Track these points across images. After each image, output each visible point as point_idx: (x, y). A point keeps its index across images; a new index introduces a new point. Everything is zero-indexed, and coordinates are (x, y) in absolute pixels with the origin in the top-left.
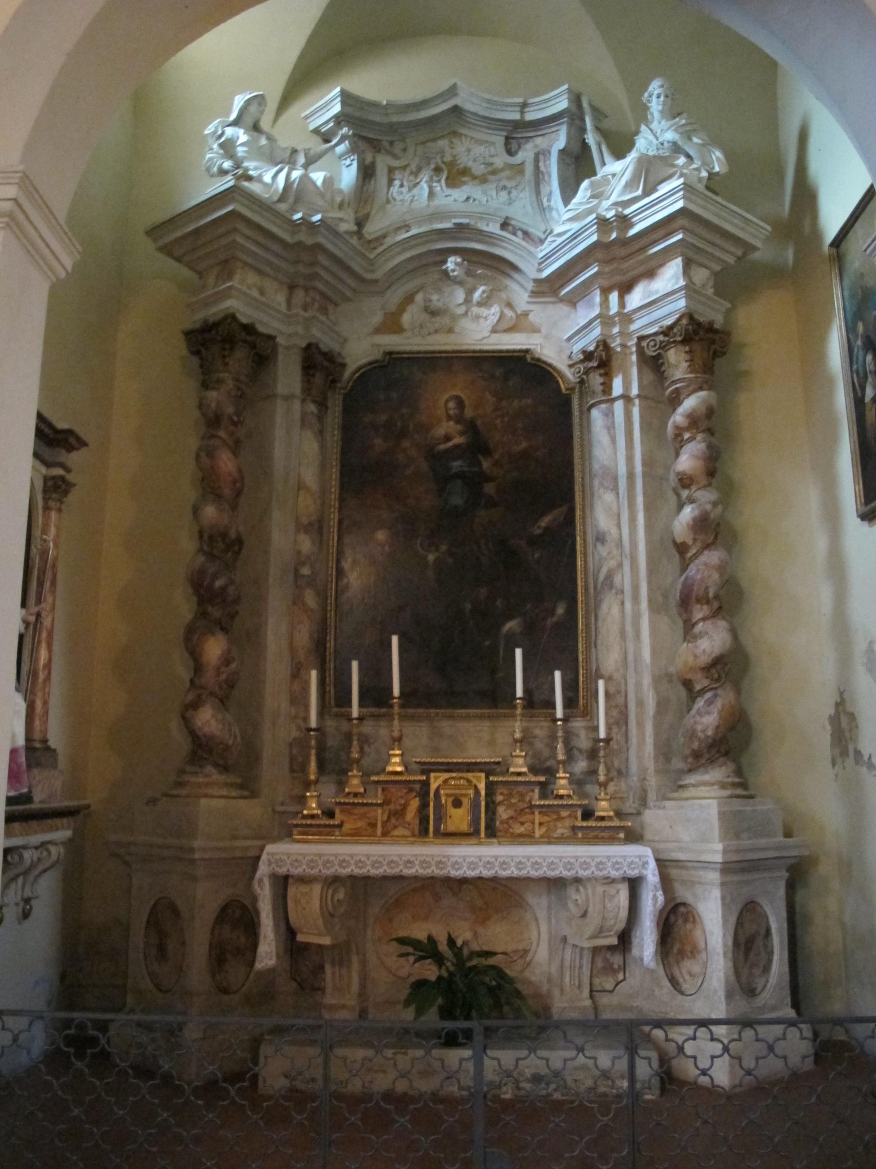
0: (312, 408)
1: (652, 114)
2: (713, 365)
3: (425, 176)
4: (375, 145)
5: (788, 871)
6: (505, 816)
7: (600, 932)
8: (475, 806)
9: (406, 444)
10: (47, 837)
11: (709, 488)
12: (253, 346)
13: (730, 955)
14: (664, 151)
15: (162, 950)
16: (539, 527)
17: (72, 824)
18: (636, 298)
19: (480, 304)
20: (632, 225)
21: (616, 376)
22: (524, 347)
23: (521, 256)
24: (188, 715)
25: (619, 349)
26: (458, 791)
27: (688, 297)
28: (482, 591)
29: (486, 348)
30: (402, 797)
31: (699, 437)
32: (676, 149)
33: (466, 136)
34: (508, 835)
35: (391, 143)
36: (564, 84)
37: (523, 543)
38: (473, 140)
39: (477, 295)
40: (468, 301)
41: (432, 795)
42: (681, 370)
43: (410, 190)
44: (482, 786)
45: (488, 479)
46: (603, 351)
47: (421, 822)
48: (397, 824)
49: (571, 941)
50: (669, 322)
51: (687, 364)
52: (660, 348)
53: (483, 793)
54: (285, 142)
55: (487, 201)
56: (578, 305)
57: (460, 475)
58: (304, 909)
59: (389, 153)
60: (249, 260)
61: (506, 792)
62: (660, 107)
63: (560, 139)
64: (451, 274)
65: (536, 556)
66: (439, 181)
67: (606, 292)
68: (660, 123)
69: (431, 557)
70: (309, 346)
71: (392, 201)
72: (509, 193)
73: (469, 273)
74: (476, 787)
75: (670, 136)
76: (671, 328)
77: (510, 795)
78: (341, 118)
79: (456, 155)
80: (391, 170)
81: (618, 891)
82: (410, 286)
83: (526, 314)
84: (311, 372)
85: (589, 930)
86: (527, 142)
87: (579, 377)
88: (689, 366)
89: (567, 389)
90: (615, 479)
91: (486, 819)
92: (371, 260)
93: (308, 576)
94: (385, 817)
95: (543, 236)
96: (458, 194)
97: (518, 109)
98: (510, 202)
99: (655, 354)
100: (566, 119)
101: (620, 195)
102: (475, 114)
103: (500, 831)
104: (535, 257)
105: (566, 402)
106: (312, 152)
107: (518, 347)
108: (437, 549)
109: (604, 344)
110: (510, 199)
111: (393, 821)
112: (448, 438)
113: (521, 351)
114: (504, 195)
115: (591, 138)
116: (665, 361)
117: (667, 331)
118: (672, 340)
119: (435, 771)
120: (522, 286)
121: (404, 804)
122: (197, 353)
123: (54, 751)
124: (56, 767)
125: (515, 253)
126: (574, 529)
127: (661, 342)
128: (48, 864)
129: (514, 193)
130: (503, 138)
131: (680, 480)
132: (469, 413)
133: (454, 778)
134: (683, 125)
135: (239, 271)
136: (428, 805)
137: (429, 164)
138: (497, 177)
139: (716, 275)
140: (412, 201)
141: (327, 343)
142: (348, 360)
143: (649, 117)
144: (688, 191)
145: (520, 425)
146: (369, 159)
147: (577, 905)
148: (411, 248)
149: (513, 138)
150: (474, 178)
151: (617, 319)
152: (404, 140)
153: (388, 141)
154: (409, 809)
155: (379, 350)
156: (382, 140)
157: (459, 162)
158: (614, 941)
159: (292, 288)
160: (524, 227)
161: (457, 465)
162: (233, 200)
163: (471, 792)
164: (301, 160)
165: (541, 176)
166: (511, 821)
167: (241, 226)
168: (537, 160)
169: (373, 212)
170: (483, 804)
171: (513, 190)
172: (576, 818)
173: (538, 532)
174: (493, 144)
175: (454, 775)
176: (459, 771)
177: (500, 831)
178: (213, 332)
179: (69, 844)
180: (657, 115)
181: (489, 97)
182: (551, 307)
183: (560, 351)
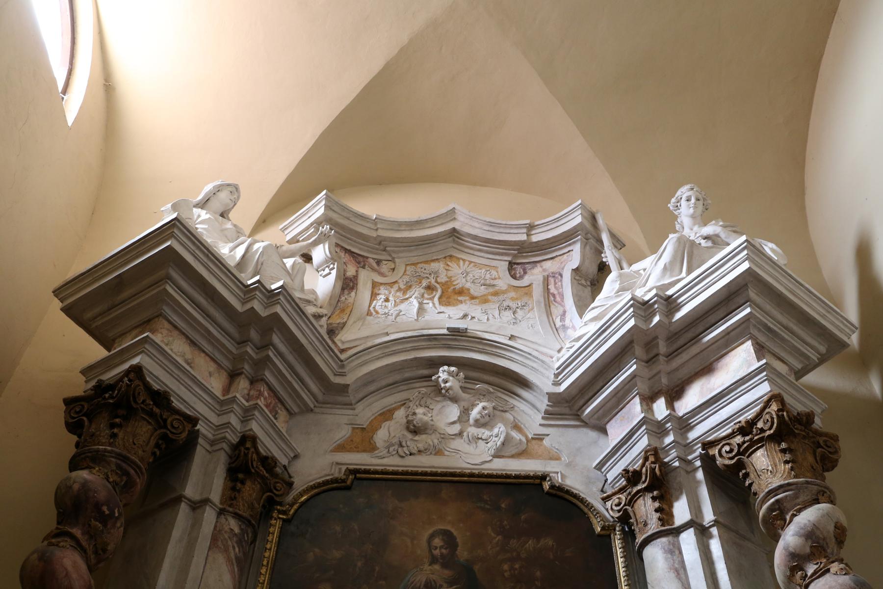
0: (233, 524)
3: (417, 291)
4: (360, 260)
19: (478, 424)
20: (678, 308)
21: (677, 499)
33: (464, 260)
35: (379, 262)
39: (475, 413)
50: (750, 415)
51: (788, 466)
55: (488, 319)
56: (608, 427)
59: (373, 269)
62: (691, 211)
66: (432, 299)
67: (648, 400)
71: (374, 313)
72: (514, 313)
76: (752, 423)
80: (375, 285)
82: (389, 401)
83: (539, 438)
84: (241, 476)
86: (533, 268)
87: (619, 511)
88: (792, 469)
89: (603, 528)
92: (342, 361)
97: (525, 230)
101: (659, 280)
102: (475, 237)
104: (549, 367)
109: (654, 453)
110: (515, 319)
113: (535, 477)
114: (508, 315)
125: (524, 365)
129: (520, 313)
130: (507, 263)
132: (462, 554)
135: (165, 332)
138: (501, 297)
140: (398, 315)
146: (351, 271)
148: (395, 353)
149: (518, 264)
150: (473, 298)
152: (393, 260)
155: (340, 469)
156: (367, 258)
157: (455, 283)
159: (233, 376)
162: (172, 236)
165: (552, 298)
168: (546, 281)
171: (518, 310)
174: (495, 267)
182: (572, 431)
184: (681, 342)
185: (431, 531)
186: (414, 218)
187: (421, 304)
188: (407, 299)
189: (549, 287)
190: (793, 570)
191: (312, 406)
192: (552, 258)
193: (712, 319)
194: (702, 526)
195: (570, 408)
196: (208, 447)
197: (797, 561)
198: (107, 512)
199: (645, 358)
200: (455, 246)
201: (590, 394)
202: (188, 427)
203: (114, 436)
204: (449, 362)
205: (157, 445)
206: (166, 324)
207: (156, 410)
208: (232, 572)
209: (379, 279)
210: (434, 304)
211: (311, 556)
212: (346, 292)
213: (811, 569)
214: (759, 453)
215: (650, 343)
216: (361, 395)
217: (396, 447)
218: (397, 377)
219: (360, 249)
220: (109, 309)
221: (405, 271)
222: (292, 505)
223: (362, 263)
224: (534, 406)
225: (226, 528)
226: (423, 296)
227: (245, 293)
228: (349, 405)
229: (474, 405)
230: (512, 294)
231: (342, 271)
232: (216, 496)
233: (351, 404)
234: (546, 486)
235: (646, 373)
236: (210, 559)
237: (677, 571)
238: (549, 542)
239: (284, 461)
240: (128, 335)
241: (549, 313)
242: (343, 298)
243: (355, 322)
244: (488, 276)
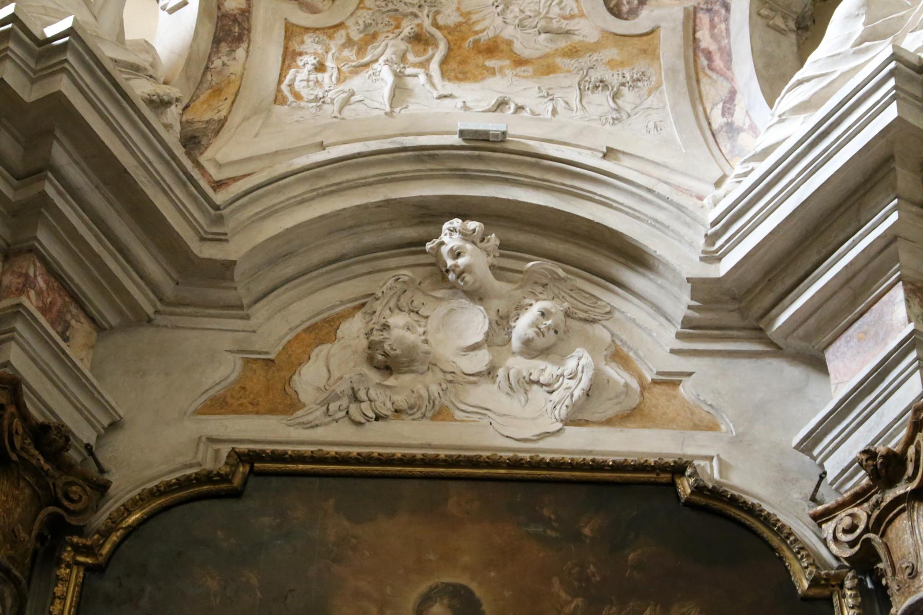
19: (530, 349)
23: (656, 224)
39: (523, 325)
55: (554, 112)
56: (829, 355)
66: (424, 65)
72: (615, 96)
79: (469, 13)
80: (291, 32)
89: (815, 582)
92: (217, 208)
110: (618, 110)
113: (660, 467)
114: (601, 101)
120: (658, 309)
129: (629, 97)
138: (585, 61)
140: (346, 102)
150: (520, 62)
157: (477, 28)
169: (234, 120)
181: (523, 88)
183: (784, 478)
185: (424, 587)
187: (399, 76)
188: (367, 65)
189: (699, 35)
191: (150, 310)
201: (789, 282)
210: (428, 75)
212: (224, 48)
216: (262, 287)
217: (344, 402)
218: (346, 244)
224: (658, 309)
229: (520, 308)
230: (611, 53)
233: (241, 307)
234: (685, 487)
242: (217, 63)
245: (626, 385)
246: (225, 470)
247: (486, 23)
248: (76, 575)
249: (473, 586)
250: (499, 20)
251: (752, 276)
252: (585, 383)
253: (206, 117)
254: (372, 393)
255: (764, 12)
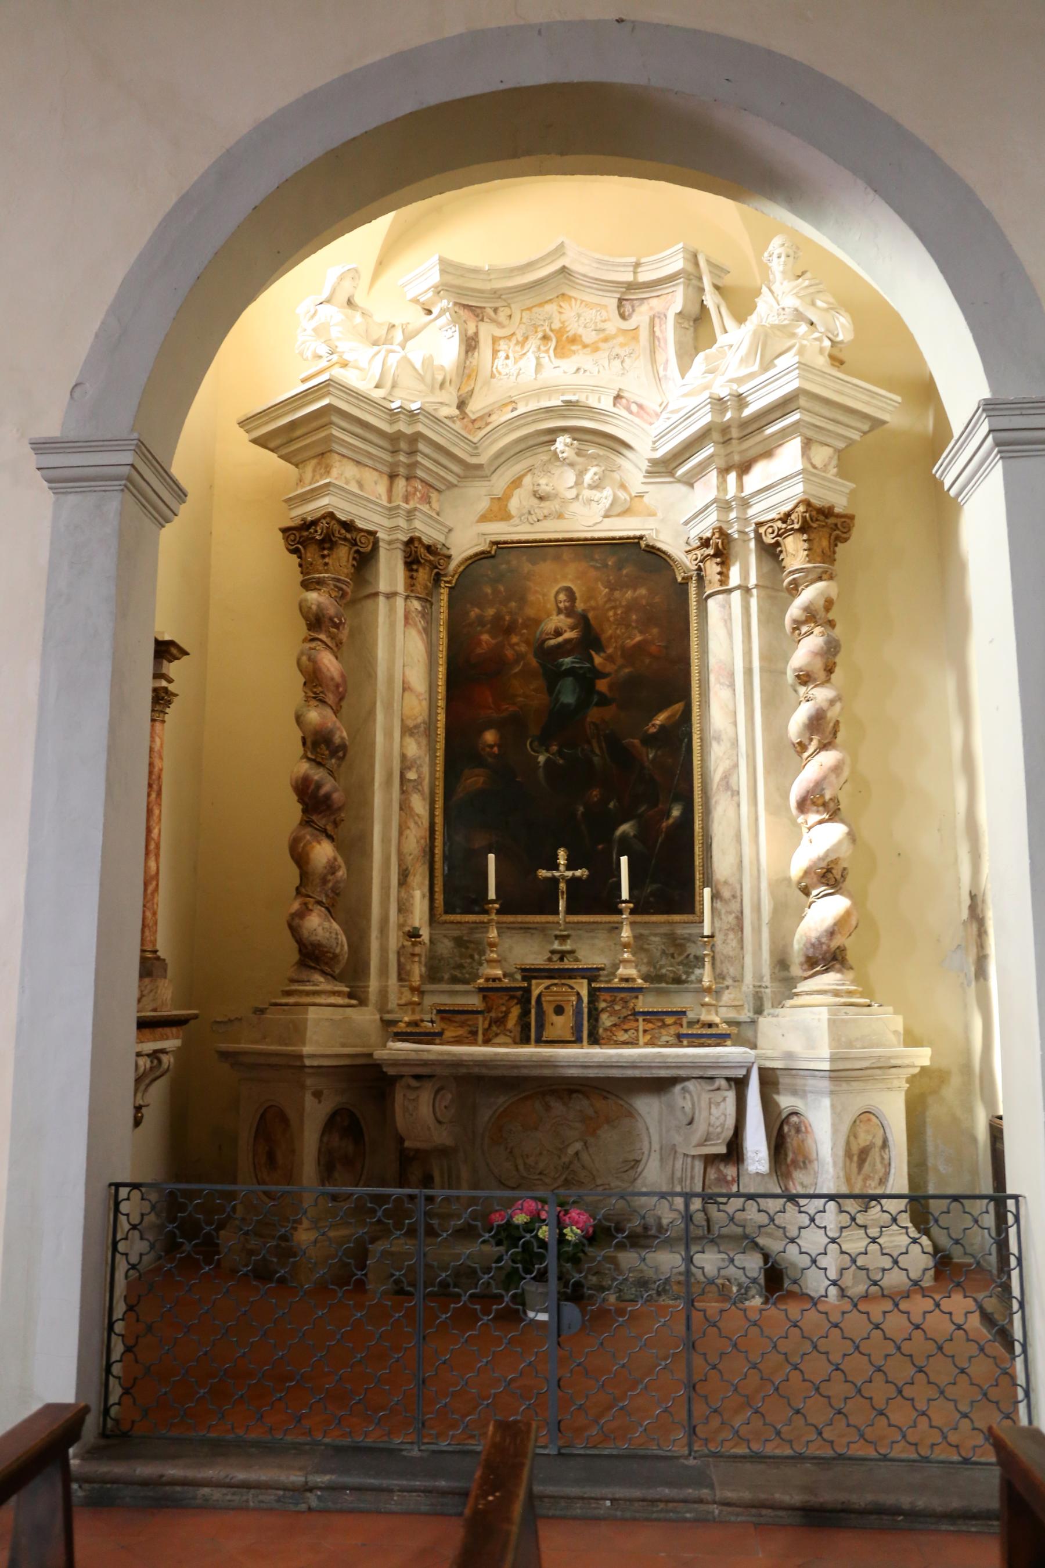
0: (416, 605)
1: (773, 274)
2: (834, 553)
3: (533, 343)
4: (477, 312)
5: (907, 1082)
6: (608, 1023)
7: (707, 1139)
8: (578, 1013)
9: (515, 639)
10: (158, 1045)
11: (828, 685)
12: (354, 543)
13: (840, 1164)
14: (785, 317)
15: (271, 1157)
16: (653, 725)
17: (181, 1033)
18: (759, 475)
19: (591, 487)
21: (734, 564)
22: (638, 533)
24: (294, 924)
25: (736, 536)
26: (559, 998)
27: (805, 481)
28: (594, 793)
29: (597, 535)
30: (503, 1004)
31: (818, 630)
32: (799, 316)
33: (576, 299)
34: (612, 1042)
35: (495, 310)
36: (677, 243)
37: (636, 741)
38: (584, 303)
39: (588, 478)
40: (578, 483)
41: (533, 1002)
42: (798, 559)
43: (516, 362)
44: (584, 993)
45: (602, 675)
46: (718, 538)
47: (523, 1029)
48: (499, 1032)
49: (681, 1150)
51: (806, 553)
52: (778, 535)
53: (585, 999)
54: (382, 316)
55: (599, 372)
56: (695, 485)
57: (571, 672)
58: (412, 1115)
59: (492, 321)
60: (344, 451)
61: (609, 999)
62: (781, 268)
63: (676, 300)
64: (560, 455)
65: (651, 756)
66: (547, 351)
67: (724, 471)
68: (782, 284)
69: (542, 759)
70: (411, 541)
71: (497, 375)
73: (579, 453)
74: (578, 994)
75: (791, 302)
76: (788, 515)
77: (613, 1002)
78: (440, 288)
80: (495, 340)
81: (724, 1099)
83: (640, 496)
84: (415, 567)
85: (696, 1138)
86: (640, 305)
89: (683, 578)
90: (732, 675)
91: (589, 1026)
93: (415, 780)
94: (486, 1026)
95: (659, 410)
96: (568, 365)
97: (631, 269)
98: (624, 373)
99: (773, 541)
100: (682, 280)
103: (603, 1039)
105: (683, 587)
106: (410, 328)
107: (631, 534)
108: (547, 751)
110: (624, 368)
111: (494, 1028)
112: (558, 633)
113: (635, 538)
114: (617, 363)
115: (711, 299)
116: (783, 549)
117: (785, 518)
118: (789, 527)
119: (536, 978)
120: (637, 466)
121: (505, 1012)
122: (295, 551)
123: (164, 960)
124: (165, 978)
126: (690, 726)
127: (779, 529)
128: (158, 1073)
130: (617, 300)
131: (798, 676)
132: (580, 606)
133: (555, 985)
134: (807, 287)
135: (337, 464)
136: (530, 1012)
137: (536, 332)
138: (610, 344)
139: (839, 452)
140: (518, 374)
141: (430, 534)
142: (453, 552)
143: (771, 277)
144: (804, 370)
145: (634, 617)
147: (684, 1113)
148: (518, 427)
149: (627, 300)
150: (585, 346)
151: (733, 503)
152: (509, 306)
153: (491, 308)
154: (511, 1016)
155: (485, 539)
156: (484, 308)
157: (568, 329)
158: (723, 1150)
160: (640, 401)
161: (568, 661)
163: (574, 998)
164: (398, 336)
165: (657, 343)
166: (614, 1029)
167: (335, 419)
170: (586, 1010)
172: (681, 1026)
173: (653, 730)
175: (556, 981)
176: (560, 977)
177: (603, 1039)
178: (312, 530)
179: (178, 1052)
180: (779, 276)
184: (749, 430)
185: (556, 589)
186: (523, 260)
187: (538, 358)
188: (525, 354)
189: (655, 329)
190: (794, 629)
191: (455, 482)
192: (658, 296)
193: (773, 417)
194: (747, 587)
195: (666, 467)
196: (387, 547)
197: (797, 624)
198: (338, 622)
199: (721, 440)
200: (566, 282)
201: (681, 461)
202: (371, 538)
203: (326, 564)
204: (564, 430)
205: (354, 559)
206: (337, 457)
207: (349, 536)
208: (422, 639)
209: (499, 332)
210: (549, 357)
211: (473, 614)
212: (470, 354)
213: (804, 629)
214: (790, 538)
215: (725, 429)
216: (493, 468)
217: (526, 516)
218: (523, 446)
219: (477, 301)
220: (288, 442)
221: (521, 318)
222: (453, 576)
223: (481, 315)
224: (637, 466)
225: (413, 609)
226: (539, 348)
227: (391, 415)
228: (486, 478)
229: (586, 470)
230: (621, 339)
231: (464, 332)
232: (400, 588)
233: (487, 477)
234: (643, 544)
235: (722, 451)
236: (407, 633)
237: (725, 621)
238: (642, 591)
239: (441, 538)
240: (308, 462)
241: (653, 361)
242: (468, 363)
243: (481, 388)
244: (599, 318)
245: (625, 499)
246: (489, 549)
247: (571, 327)
248: (447, 590)
249: (572, 587)
250: (576, 324)
251: (668, 457)
252: (610, 502)
253: (466, 390)
254: (536, 511)
255: (680, 321)
